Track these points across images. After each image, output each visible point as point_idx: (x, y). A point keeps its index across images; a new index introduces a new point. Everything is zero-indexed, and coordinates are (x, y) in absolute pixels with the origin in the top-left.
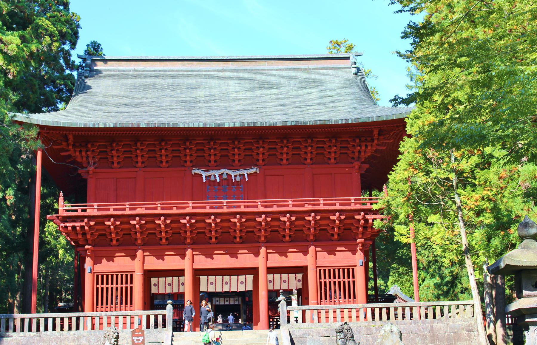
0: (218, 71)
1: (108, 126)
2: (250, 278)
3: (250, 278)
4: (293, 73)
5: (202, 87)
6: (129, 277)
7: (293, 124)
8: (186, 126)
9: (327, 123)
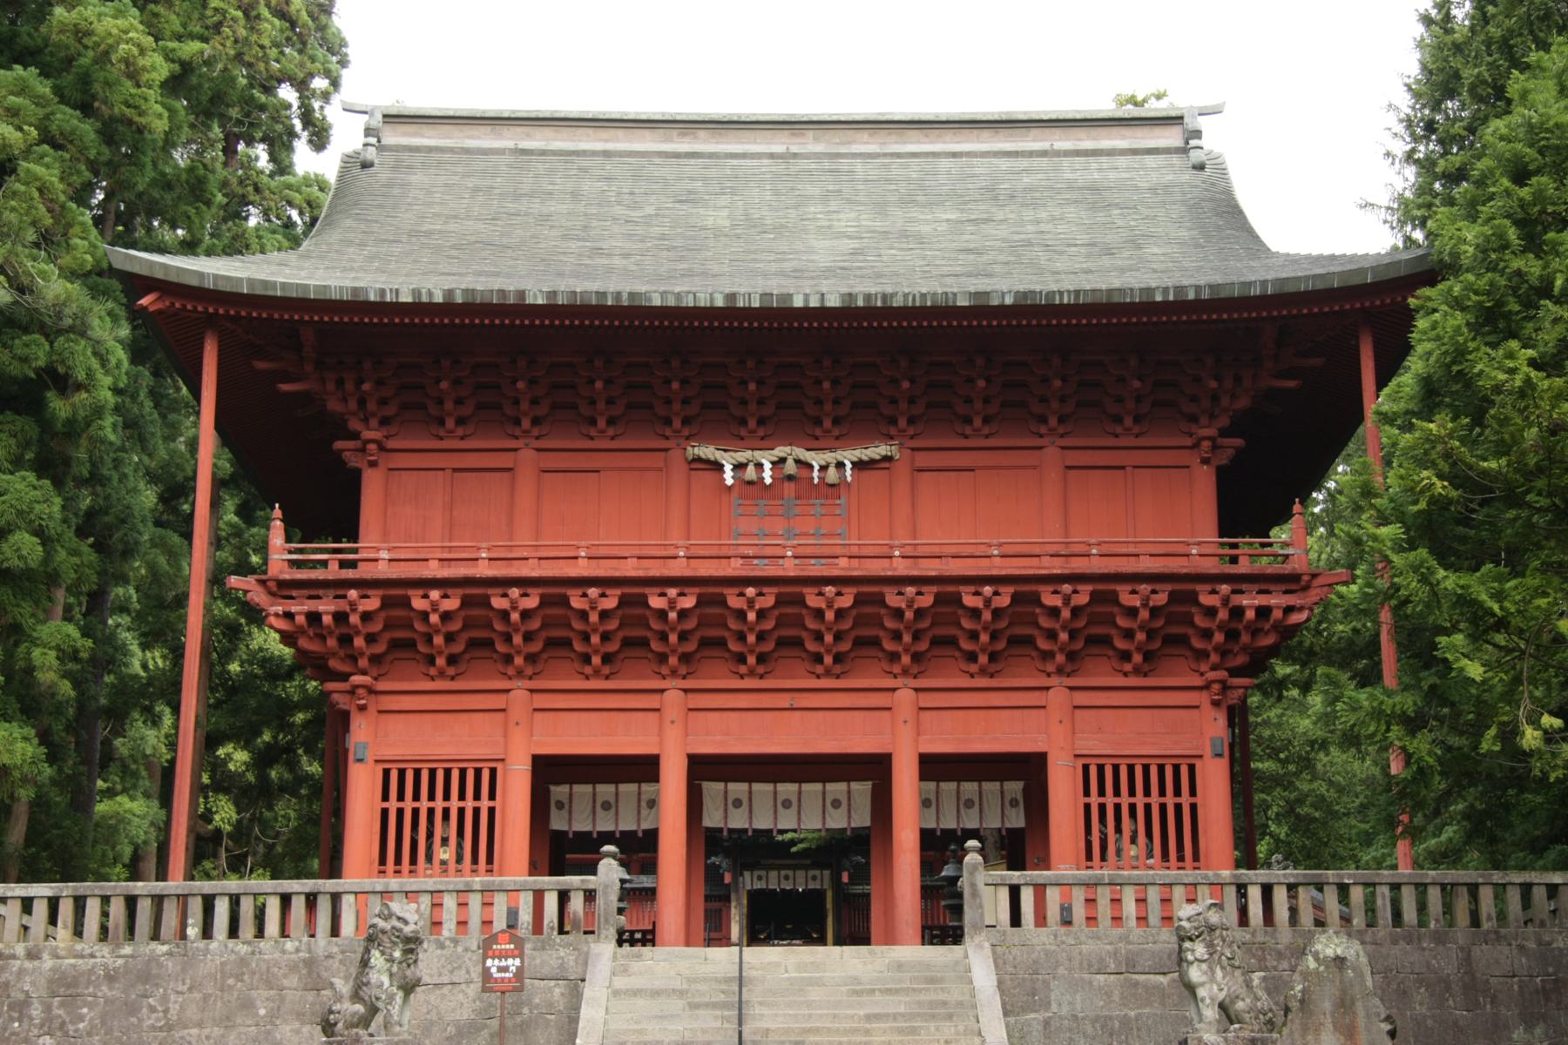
0: (772, 156)
1: (425, 299)
2: (862, 789)
3: (862, 789)
4: (1004, 164)
5: (724, 200)
6: (485, 779)
7: (1009, 301)
8: (671, 302)
9: (1116, 299)
